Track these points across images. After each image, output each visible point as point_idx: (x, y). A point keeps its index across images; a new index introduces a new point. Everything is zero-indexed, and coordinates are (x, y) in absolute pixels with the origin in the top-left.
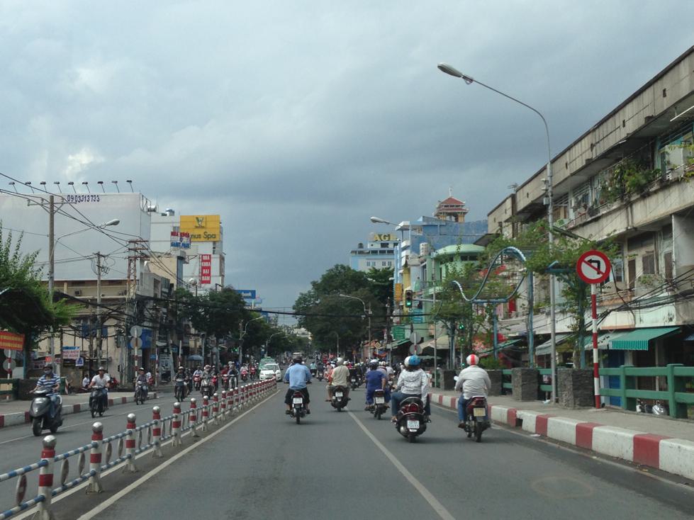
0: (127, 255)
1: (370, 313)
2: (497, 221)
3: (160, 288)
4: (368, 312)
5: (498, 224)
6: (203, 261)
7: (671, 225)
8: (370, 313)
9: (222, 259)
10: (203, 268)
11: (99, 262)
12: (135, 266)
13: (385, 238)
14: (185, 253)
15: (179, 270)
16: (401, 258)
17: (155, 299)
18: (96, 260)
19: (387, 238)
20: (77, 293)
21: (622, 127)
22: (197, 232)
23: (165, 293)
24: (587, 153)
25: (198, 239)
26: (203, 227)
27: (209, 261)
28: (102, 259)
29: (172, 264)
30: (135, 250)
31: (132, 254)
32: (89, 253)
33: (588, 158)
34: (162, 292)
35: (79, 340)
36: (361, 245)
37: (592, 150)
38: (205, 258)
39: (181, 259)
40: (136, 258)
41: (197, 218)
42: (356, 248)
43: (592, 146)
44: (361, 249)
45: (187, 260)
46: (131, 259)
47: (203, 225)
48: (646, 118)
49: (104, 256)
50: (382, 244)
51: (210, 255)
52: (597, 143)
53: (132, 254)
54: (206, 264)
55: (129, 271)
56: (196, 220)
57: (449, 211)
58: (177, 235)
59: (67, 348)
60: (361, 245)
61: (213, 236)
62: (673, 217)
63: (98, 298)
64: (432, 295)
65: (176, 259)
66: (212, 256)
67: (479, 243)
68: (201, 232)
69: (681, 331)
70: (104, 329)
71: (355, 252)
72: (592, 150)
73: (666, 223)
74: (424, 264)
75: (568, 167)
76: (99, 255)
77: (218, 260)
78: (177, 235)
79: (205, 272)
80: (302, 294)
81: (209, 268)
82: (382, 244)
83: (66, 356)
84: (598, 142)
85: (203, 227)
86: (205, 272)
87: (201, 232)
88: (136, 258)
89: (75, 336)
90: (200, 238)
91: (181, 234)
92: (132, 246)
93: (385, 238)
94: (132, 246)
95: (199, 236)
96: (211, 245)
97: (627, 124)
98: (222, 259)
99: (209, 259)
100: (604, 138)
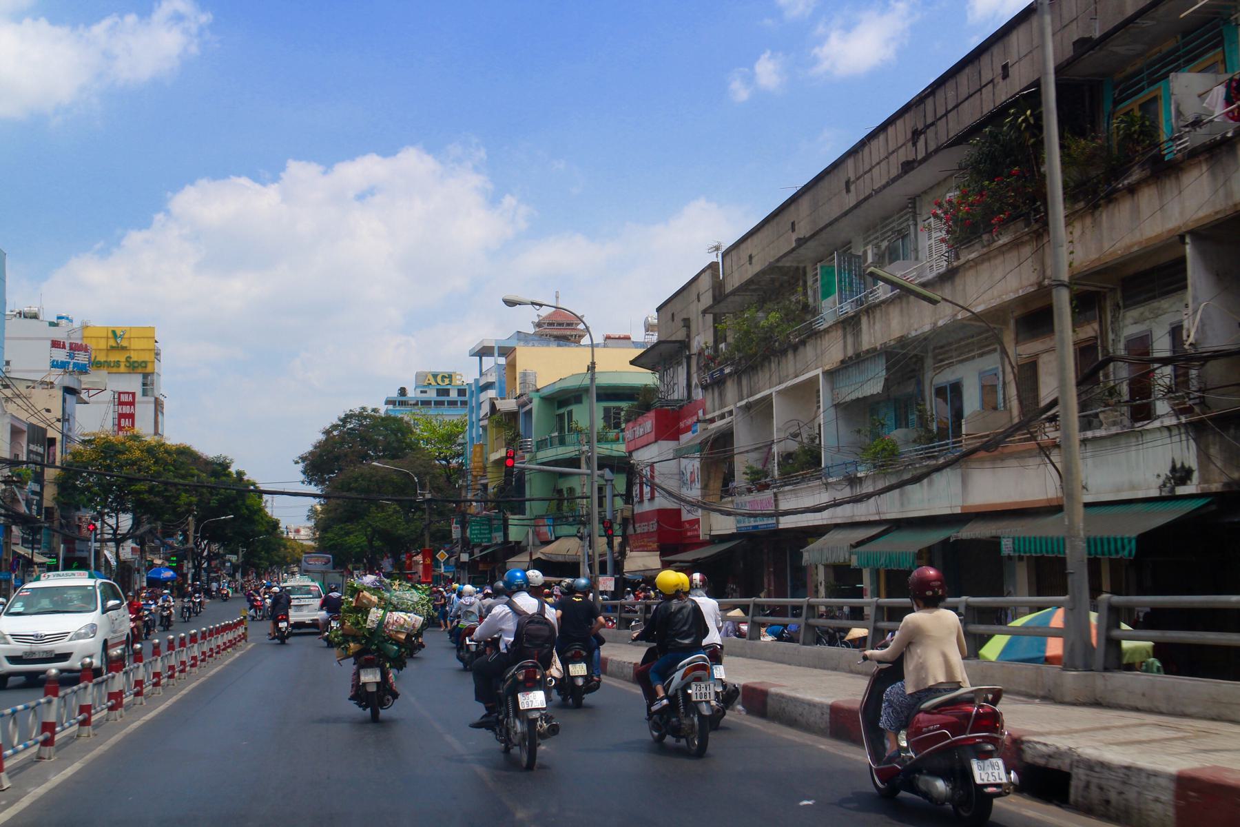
2: (678, 319)
3: (24, 445)
4: (423, 495)
5: (682, 324)
6: (121, 403)
7: (1182, 260)
9: (158, 406)
10: (121, 416)
13: (443, 381)
14: (80, 381)
16: (480, 405)
19: (447, 381)
21: (999, 79)
22: (114, 357)
23: (37, 454)
24: (902, 151)
25: (115, 370)
26: (124, 349)
27: (132, 404)
33: (1075, 38)
34: (30, 452)
36: (403, 391)
37: (914, 144)
38: (124, 398)
41: (114, 332)
42: (394, 394)
43: (916, 134)
45: (84, 396)
47: (125, 343)
48: (1074, 43)
50: (437, 390)
51: (134, 394)
52: (928, 127)
54: (126, 409)
56: (110, 335)
57: (555, 333)
58: (64, 347)
61: (144, 364)
62: (1188, 240)
67: (643, 361)
68: (121, 357)
69: (1214, 507)
70: (78, 545)
72: (914, 144)
73: (1165, 258)
74: (527, 408)
75: (852, 188)
77: (152, 406)
78: (64, 347)
80: (303, 459)
81: (131, 416)
82: (437, 390)
84: (933, 124)
87: (121, 357)
91: (71, 344)
93: (443, 381)
95: (118, 364)
97: (702, 298)
99: (131, 399)
100: (947, 112)
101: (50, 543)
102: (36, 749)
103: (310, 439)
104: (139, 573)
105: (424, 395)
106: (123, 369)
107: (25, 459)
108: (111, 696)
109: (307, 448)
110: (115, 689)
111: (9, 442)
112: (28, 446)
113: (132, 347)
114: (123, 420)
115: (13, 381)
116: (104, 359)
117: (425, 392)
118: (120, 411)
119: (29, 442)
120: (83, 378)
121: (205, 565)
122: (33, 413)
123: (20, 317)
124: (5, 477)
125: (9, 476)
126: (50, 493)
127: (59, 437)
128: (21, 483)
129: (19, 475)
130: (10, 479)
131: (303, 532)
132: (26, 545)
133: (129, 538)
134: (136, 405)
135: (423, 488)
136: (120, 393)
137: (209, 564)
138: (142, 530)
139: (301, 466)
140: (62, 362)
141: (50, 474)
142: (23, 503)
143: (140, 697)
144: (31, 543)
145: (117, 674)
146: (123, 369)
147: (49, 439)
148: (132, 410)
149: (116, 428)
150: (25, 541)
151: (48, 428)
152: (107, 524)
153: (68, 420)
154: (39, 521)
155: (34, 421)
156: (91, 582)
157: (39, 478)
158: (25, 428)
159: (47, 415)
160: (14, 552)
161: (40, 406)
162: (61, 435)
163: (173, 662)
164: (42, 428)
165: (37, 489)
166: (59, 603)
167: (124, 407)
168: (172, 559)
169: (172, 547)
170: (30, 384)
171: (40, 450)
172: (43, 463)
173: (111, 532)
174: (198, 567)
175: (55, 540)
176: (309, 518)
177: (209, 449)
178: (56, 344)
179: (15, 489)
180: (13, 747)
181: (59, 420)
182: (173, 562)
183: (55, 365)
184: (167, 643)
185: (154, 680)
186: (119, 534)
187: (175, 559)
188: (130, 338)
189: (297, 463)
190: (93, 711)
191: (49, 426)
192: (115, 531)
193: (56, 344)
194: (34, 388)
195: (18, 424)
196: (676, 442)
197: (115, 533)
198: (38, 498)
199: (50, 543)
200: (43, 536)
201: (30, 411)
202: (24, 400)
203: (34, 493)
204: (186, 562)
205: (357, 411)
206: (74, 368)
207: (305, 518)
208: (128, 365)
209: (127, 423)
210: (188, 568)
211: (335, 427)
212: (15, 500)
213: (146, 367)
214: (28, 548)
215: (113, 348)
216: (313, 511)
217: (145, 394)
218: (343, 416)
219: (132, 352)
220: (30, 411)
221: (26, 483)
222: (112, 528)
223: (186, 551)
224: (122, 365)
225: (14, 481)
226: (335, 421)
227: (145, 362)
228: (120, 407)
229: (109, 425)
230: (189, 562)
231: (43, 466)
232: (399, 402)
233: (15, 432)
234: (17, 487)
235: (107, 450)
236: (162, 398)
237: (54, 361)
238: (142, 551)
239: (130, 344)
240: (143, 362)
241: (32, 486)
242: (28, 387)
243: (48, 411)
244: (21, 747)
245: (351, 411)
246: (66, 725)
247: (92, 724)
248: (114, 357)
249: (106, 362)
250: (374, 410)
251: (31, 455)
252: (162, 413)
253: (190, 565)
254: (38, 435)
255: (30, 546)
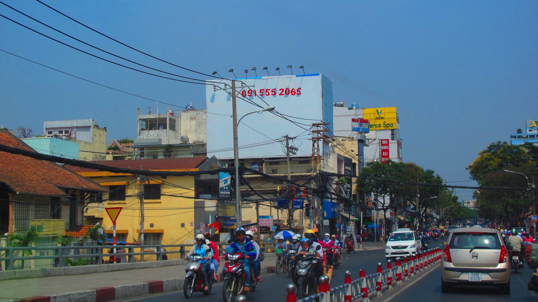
0: (311, 136)
1: (534, 186)
3: (343, 167)
4: (531, 186)
6: (382, 145)
8: (534, 186)
10: (383, 151)
11: (287, 144)
12: (318, 146)
14: (365, 136)
15: (360, 154)
17: (339, 175)
18: (285, 142)
20: (274, 171)
22: (378, 122)
23: (348, 170)
25: (379, 128)
26: (382, 118)
27: (387, 145)
28: (290, 141)
29: (354, 146)
30: (318, 132)
31: (316, 135)
32: (279, 136)
34: (345, 170)
35: (274, 211)
36: (519, 131)
38: (384, 142)
39: (362, 142)
40: (319, 139)
44: (520, 135)
45: (367, 142)
46: (315, 140)
49: (292, 139)
51: (388, 140)
53: (316, 135)
54: (385, 148)
55: (313, 150)
59: (263, 217)
60: (519, 131)
63: (289, 175)
64: (445, 245)
65: (357, 142)
66: (390, 141)
68: (381, 122)
70: (367, 211)
71: (515, 137)
76: (287, 138)
79: (385, 154)
81: (387, 151)
83: (262, 224)
85: (382, 118)
86: (385, 154)
88: (319, 139)
89: (271, 207)
90: (380, 127)
92: (315, 128)
94: (315, 128)
95: (380, 125)
96: (390, 132)
98: (399, 145)
99: (387, 142)
101: (356, 211)
102: (386, 286)
103: (473, 158)
104: (395, 224)
105: (531, 132)
106: (382, 128)
107: (343, 173)
108: (397, 275)
109: (471, 164)
110: (398, 272)
111: (337, 166)
112: (345, 167)
113: (386, 117)
114: (384, 152)
115: (337, 138)
116: (374, 124)
117: (531, 131)
118: (382, 148)
119: (345, 165)
120: (367, 135)
121: (424, 220)
122: (346, 152)
123: (336, 106)
124: (336, 182)
125: (338, 181)
126: (354, 187)
127: (357, 162)
128: (343, 184)
129: (341, 181)
130: (339, 183)
131: (471, 204)
132: (346, 212)
133: (389, 208)
134: (390, 145)
135: (531, 182)
136: (382, 140)
137: (426, 220)
138: (394, 205)
139: (469, 170)
140: (357, 128)
141: (354, 180)
142: (344, 193)
143: (379, 292)
144: (349, 211)
145: (399, 267)
146: (382, 128)
147: (353, 163)
148: (388, 148)
149: (381, 156)
150: (345, 210)
151: (353, 159)
152: (379, 202)
153: (361, 155)
154: (351, 201)
155: (346, 156)
156: (411, 232)
157: (350, 182)
158: (343, 160)
159: (352, 153)
160: (342, 215)
161: (349, 149)
162: (358, 162)
163: (390, 275)
164: (350, 159)
165: (349, 186)
166: (403, 237)
167: (384, 146)
168: (409, 217)
169: (408, 212)
170: (343, 138)
171: (350, 169)
172: (352, 174)
173: (382, 205)
174: (421, 222)
175: (358, 209)
176: (474, 197)
177: (426, 167)
178: (354, 120)
179: (341, 187)
180: (369, 289)
181: (357, 155)
182: (409, 219)
183: (354, 129)
184: (377, 268)
185: (388, 282)
186: (385, 206)
187: (410, 217)
188: (385, 113)
189: (467, 169)
190: (382, 285)
191: (353, 157)
192: (383, 206)
193: (354, 120)
194: (345, 140)
195: (340, 158)
196: (320, 297)
197: (383, 206)
198: (350, 190)
199: (356, 211)
200: (352, 208)
201: (344, 151)
202: (342, 146)
203: (348, 188)
204: (415, 219)
205: (496, 143)
206: (362, 130)
207: (472, 197)
208: (384, 126)
209: (386, 154)
210: (417, 222)
211: (485, 152)
212: (341, 191)
213: (392, 126)
214: (347, 213)
215: (377, 118)
216: (475, 193)
217: (393, 139)
218: (489, 146)
219: (386, 119)
220: (344, 151)
221: (345, 184)
222: (382, 203)
223: (415, 213)
224: (382, 126)
225: (340, 184)
226: (486, 149)
227: (392, 124)
228: (382, 147)
229: (378, 155)
230: (417, 219)
231: (351, 177)
232: (518, 136)
233: (339, 162)
234: (341, 186)
235: (375, 166)
236: (400, 140)
237: (353, 128)
238: (395, 214)
239: (385, 116)
240: (391, 124)
241: (347, 185)
242: (343, 140)
243: (353, 151)
244: (371, 290)
245: (493, 143)
246: (384, 284)
247: (382, 290)
248: (378, 122)
249: (374, 125)
250: (505, 143)
251: (346, 172)
252: (401, 148)
253: (418, 221)
254: (348, 162)
255: (348, 212)
